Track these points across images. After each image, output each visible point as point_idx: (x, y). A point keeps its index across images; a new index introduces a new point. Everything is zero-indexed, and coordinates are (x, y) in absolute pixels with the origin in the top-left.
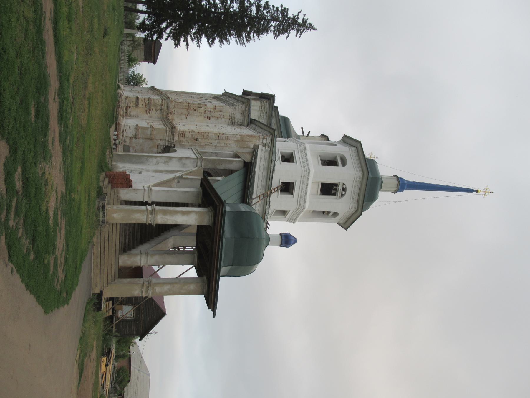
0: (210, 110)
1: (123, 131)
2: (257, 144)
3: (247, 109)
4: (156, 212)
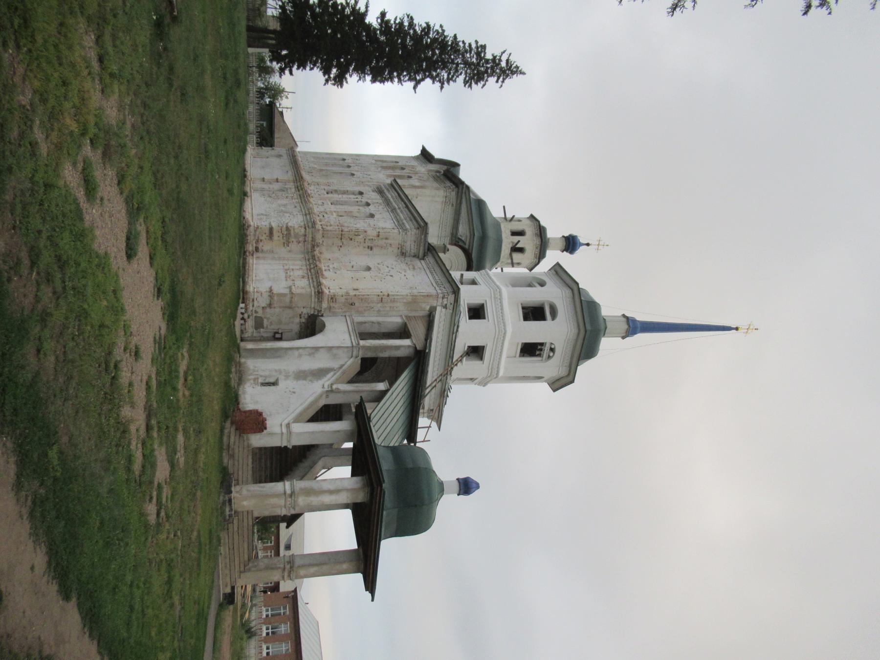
0: (371, 238)
1: (253, 300)
2: (435, 305)
3: (423, 237)
4: (296, 496)
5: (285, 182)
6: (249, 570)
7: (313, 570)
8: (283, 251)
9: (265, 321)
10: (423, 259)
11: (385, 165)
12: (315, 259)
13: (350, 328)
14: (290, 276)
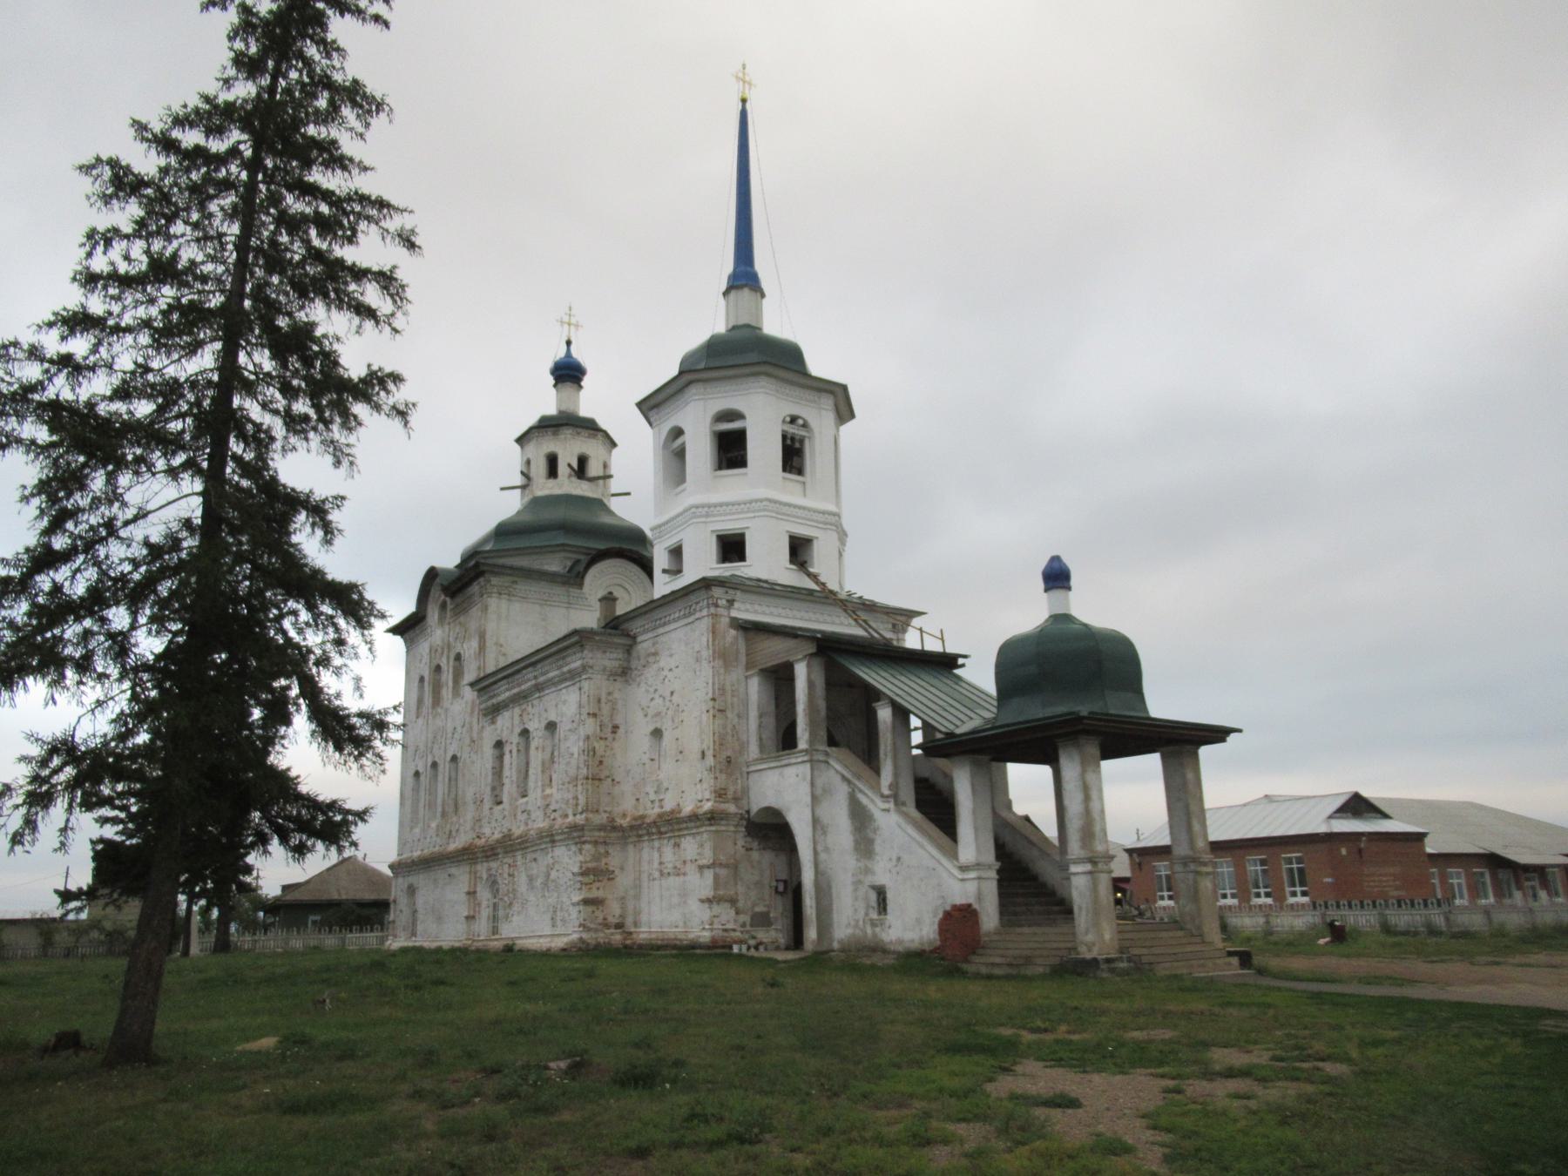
0: (598, 728)
1: (725, 930)
2: (727, 620)
3: (597, 638)
5: (475, 877)
6: (1199, 928)
7: (1196, 827)
8: (624, 881)
9: (758, 909)
10: (634, 638)
11: (428, 700)
12: (640, 826)
13: (772, 765)
14: (675, 867)
